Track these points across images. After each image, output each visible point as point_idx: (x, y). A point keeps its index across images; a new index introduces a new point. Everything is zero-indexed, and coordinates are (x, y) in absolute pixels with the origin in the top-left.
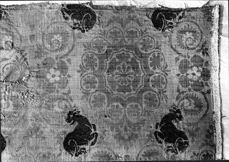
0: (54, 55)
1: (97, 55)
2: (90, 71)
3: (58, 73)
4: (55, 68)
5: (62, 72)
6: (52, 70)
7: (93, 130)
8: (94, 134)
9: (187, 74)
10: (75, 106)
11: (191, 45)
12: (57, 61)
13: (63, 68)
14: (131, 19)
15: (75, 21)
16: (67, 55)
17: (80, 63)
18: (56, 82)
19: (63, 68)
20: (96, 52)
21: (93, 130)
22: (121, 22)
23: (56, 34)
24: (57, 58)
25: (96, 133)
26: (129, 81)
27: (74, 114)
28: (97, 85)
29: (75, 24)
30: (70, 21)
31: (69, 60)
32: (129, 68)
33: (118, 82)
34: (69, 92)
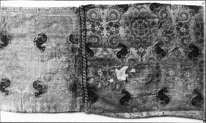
0: (183, 22)
1: (200, 23)
2: (127, 27)
3: (185, 29)
4: (183, 27)
5: (186, 29)
6: (112, 27)
7: (200, 52)
8: (200, 53)
9: (115, 29)
10: (192, 42)
11: (96, 18)
12: (184, 24)
13: (187, 27)
14: (142, 8)
15: (190, 10)
16: (188, 22)
17: (193, 26)
18: (97, 31)
19: (187, 27)
20: (200, 22)
21: (200, 52)
22: (138, 9)
23: (184, 14)
24: (184, 23)
25: (201, 53)
26: (144, 31)
27: (192, 45)
28: (131, 33)
29: (190, 11)
30: (188, 9)
31: (189, 24)
32: (143, 26)
33: (139, 31)
34: (190, 36)
